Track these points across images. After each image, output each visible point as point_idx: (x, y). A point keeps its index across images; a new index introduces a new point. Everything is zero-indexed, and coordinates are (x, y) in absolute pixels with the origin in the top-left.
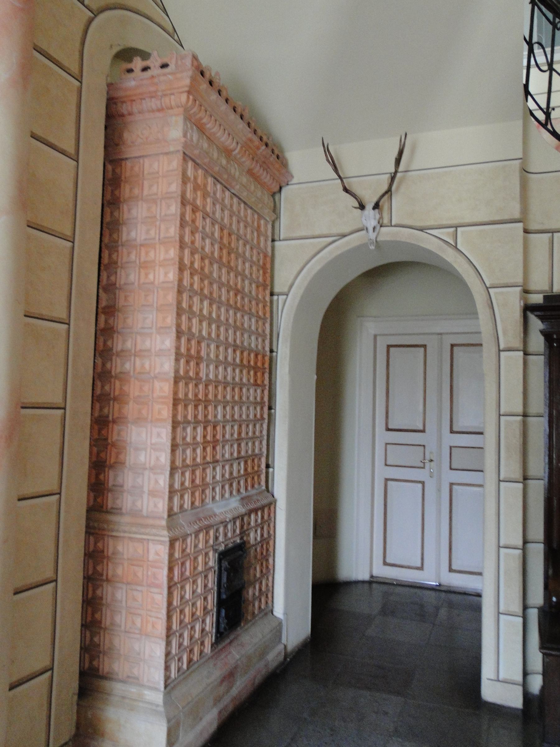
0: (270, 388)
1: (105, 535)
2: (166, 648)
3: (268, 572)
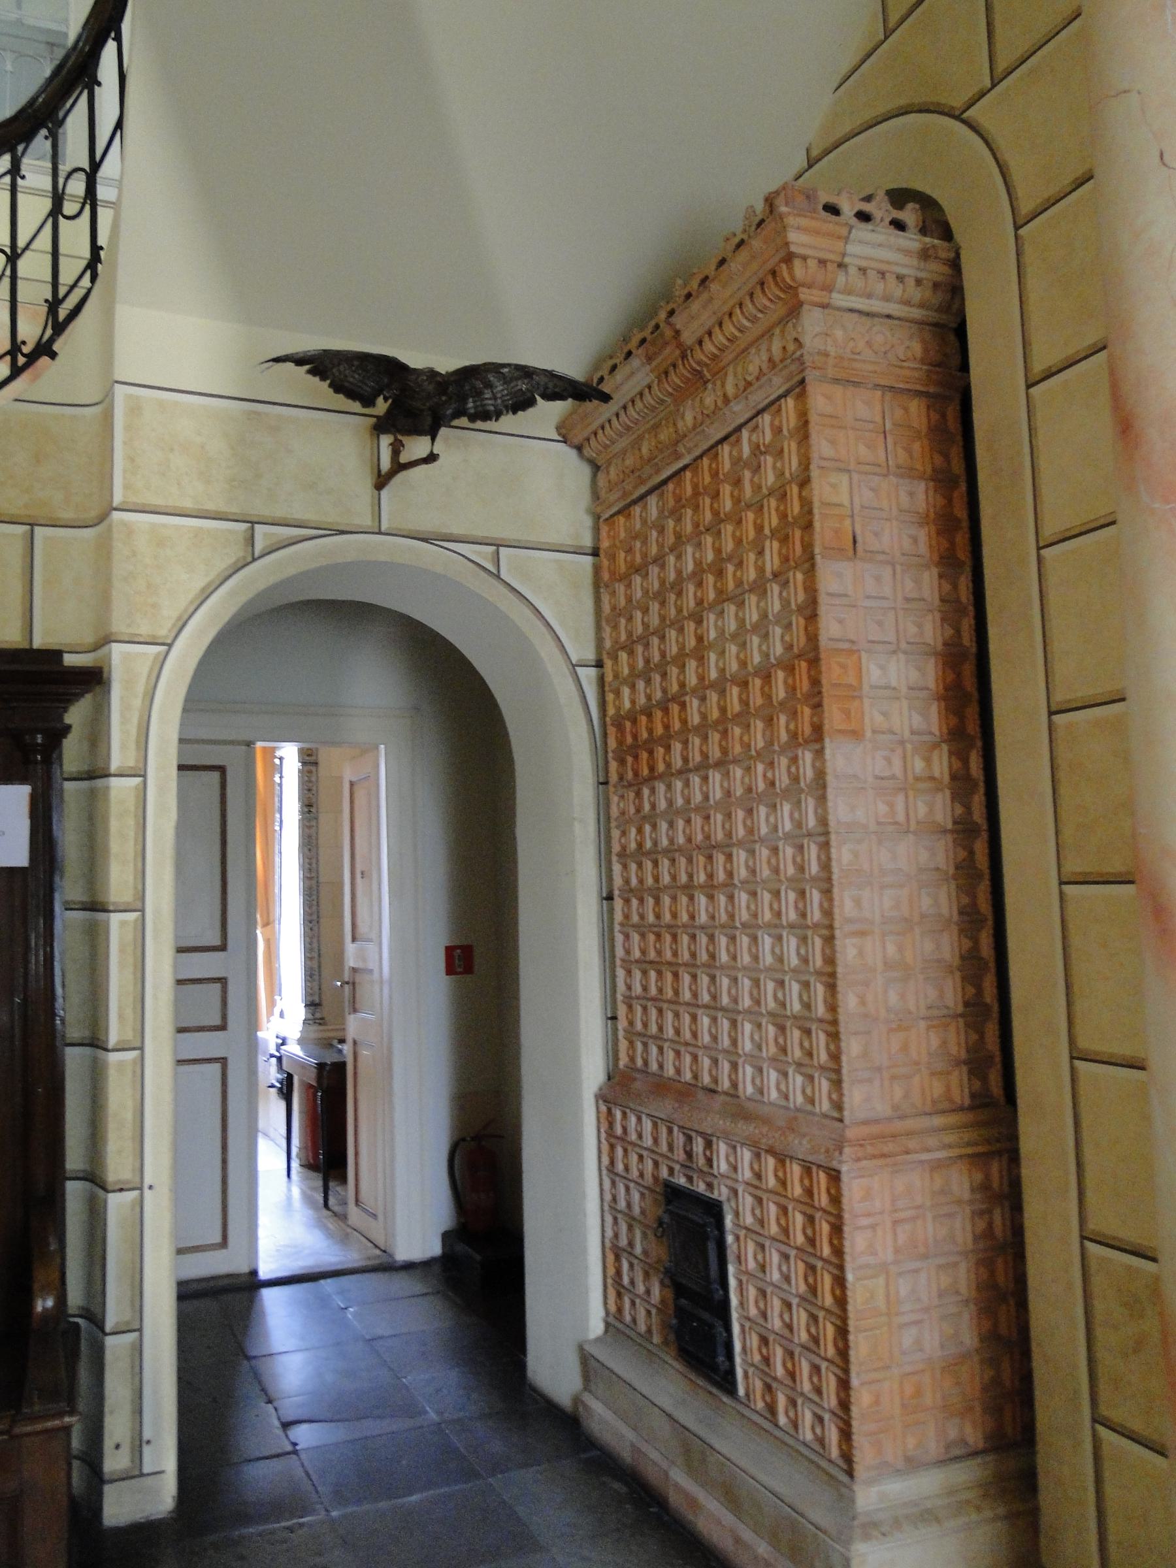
0: (613, 963)
1: (972, 1108)
2: (825, 810)
3: (615, 1252)
